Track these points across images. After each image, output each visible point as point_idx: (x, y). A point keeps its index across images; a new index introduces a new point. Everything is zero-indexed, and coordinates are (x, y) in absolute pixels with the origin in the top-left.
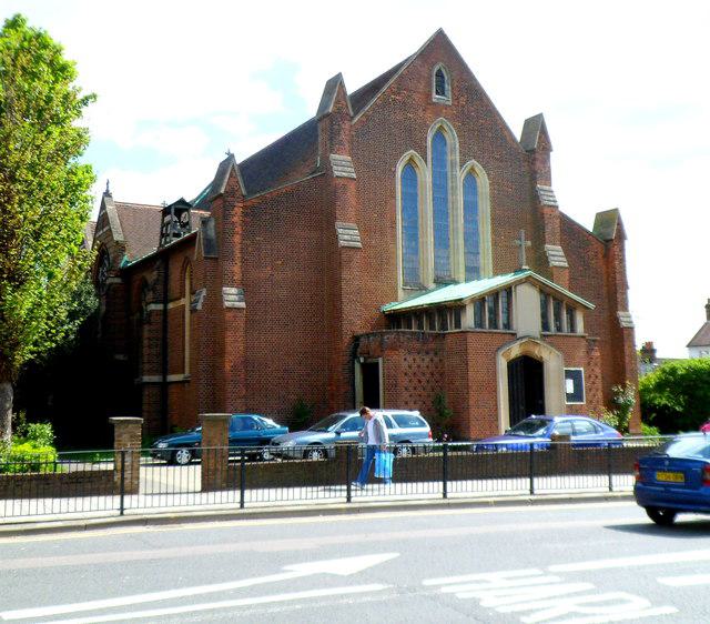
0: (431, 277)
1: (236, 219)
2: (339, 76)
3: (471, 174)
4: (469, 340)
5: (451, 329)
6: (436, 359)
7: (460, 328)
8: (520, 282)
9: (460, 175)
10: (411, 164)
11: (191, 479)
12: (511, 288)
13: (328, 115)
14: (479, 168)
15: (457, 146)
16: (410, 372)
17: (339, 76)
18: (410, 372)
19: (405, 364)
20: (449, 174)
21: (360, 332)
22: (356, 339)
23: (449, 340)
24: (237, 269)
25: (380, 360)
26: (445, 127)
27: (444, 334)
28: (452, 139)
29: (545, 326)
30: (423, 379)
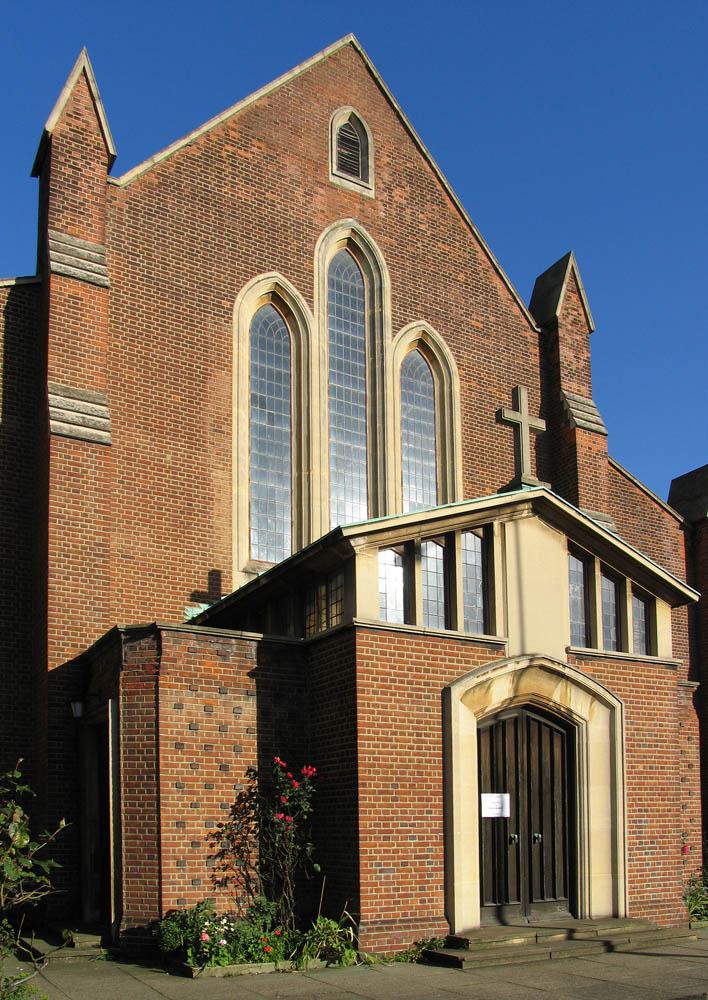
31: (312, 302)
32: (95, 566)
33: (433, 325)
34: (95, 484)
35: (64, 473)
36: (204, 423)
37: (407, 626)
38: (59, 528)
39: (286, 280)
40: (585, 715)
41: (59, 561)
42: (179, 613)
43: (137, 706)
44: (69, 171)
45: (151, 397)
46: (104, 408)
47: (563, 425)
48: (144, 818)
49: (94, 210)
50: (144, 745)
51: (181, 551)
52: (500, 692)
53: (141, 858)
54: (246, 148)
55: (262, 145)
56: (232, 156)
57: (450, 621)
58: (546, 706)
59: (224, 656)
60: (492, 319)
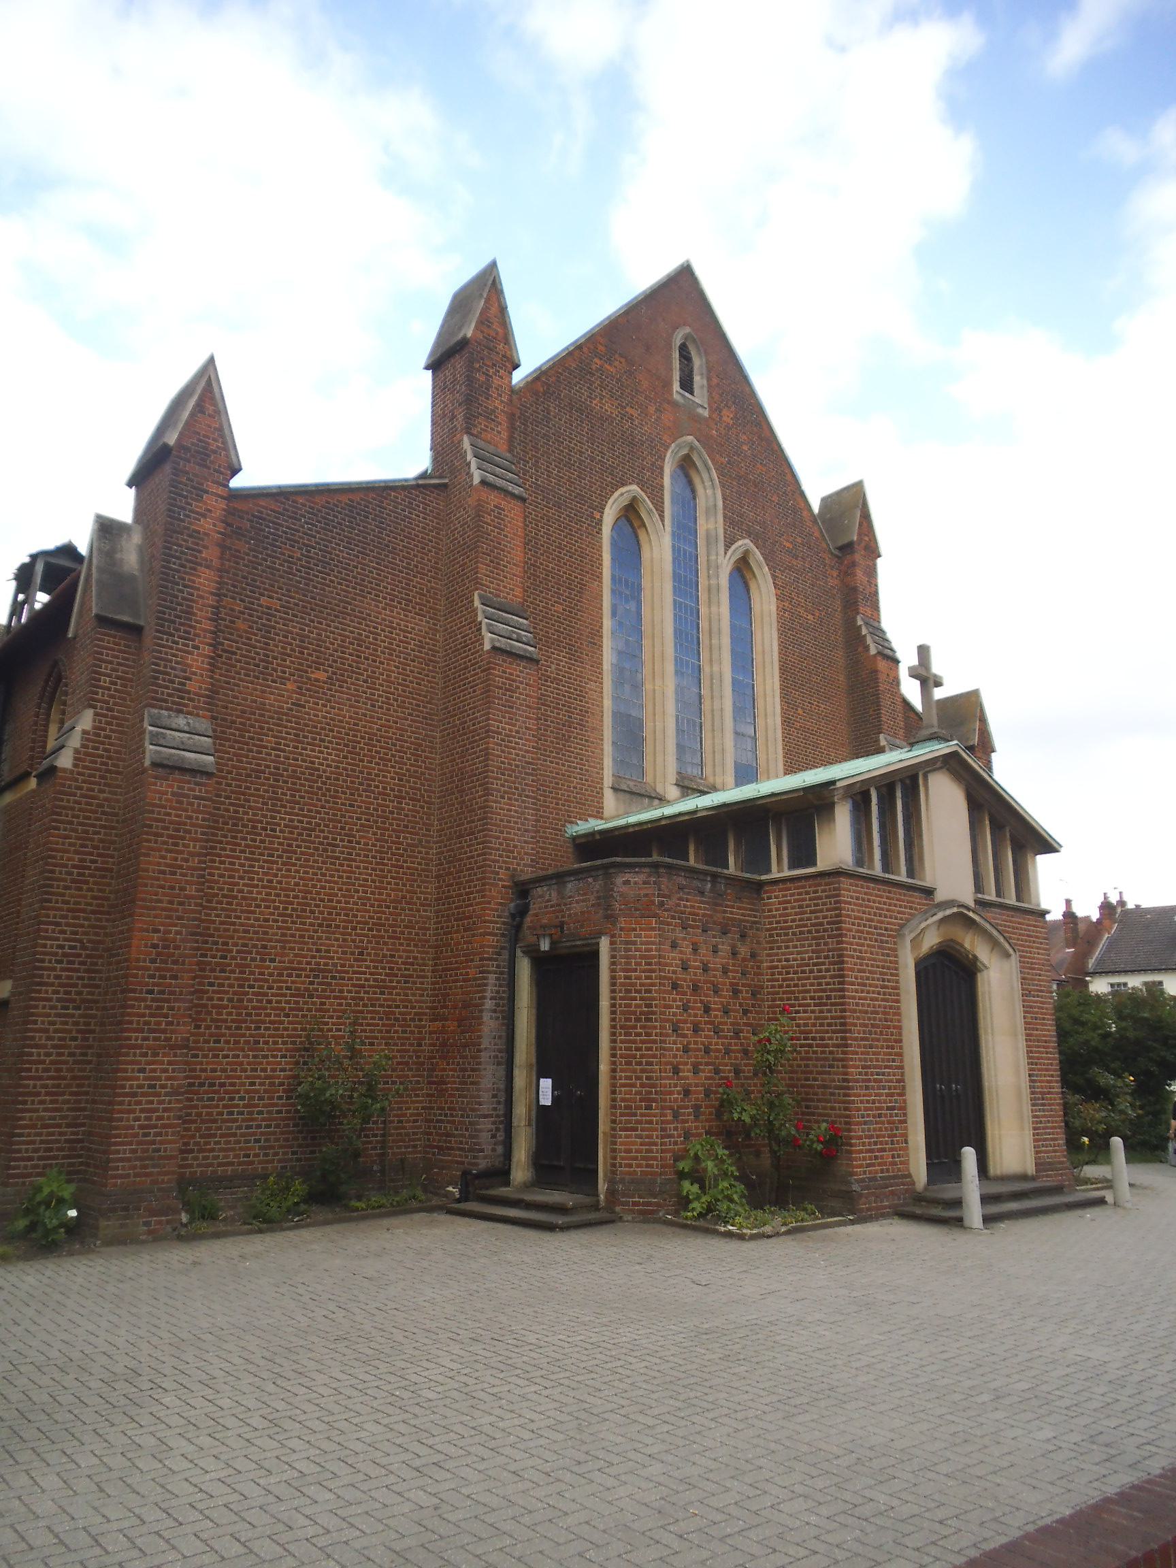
0: (672, 777)
1: (206, 525)
2: (493, 265)
3: (742, 568)
4: (846, 896)
5: (780, 869)
6: (744, 951)
7: (811, 860)
8: (931, 765)
9: (726, 564)
10: (630, 512)
11: (771, 749)
12: (914, 778)
13: (463, 344)
14: (757, 556)
15: (720, 504)
16: (685, 980)
17: (493, 265)
18: (685, 980)
19: (673, 957)
20: (702, 559)
21: (528, 873)
22: (523, 890)
23: (773, 899)
24: (197, 661)
25: (604, 944)
26: (695, 458)
27: (760, 886)
28: (709, 493)
29: (979, 887)
30: (715, 1001)
31: (663, 512)
32: (526, 784)
33: (755, 544)
34: (525, 700)
35: (501, 688)
36: (581, 634)
37: (910, 881)
38: (497, 744)
39: (643, 494)
40: (986, 962)
41: (496, 779)
42: (560, 830)
43: (634, 943)
44: (483, 378)
45: (330, 564)
46: (525, 621)
47: (860, 649)
48: (640, 1064)
49: (502, 418)
50: (642, 985)
51: (563, 765)
52: (931, 940)
53: (637, 1108)
54: (610, 361)
55: (623, 360)
56: (600, 369)
57: (886, 867)
58: (958, 951)
59: (702, 893)
60: (799, 540)
